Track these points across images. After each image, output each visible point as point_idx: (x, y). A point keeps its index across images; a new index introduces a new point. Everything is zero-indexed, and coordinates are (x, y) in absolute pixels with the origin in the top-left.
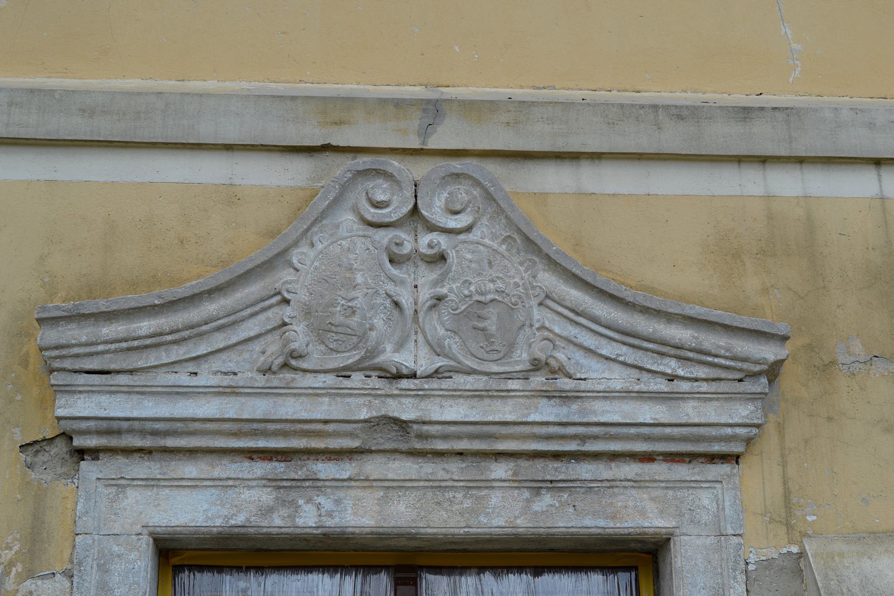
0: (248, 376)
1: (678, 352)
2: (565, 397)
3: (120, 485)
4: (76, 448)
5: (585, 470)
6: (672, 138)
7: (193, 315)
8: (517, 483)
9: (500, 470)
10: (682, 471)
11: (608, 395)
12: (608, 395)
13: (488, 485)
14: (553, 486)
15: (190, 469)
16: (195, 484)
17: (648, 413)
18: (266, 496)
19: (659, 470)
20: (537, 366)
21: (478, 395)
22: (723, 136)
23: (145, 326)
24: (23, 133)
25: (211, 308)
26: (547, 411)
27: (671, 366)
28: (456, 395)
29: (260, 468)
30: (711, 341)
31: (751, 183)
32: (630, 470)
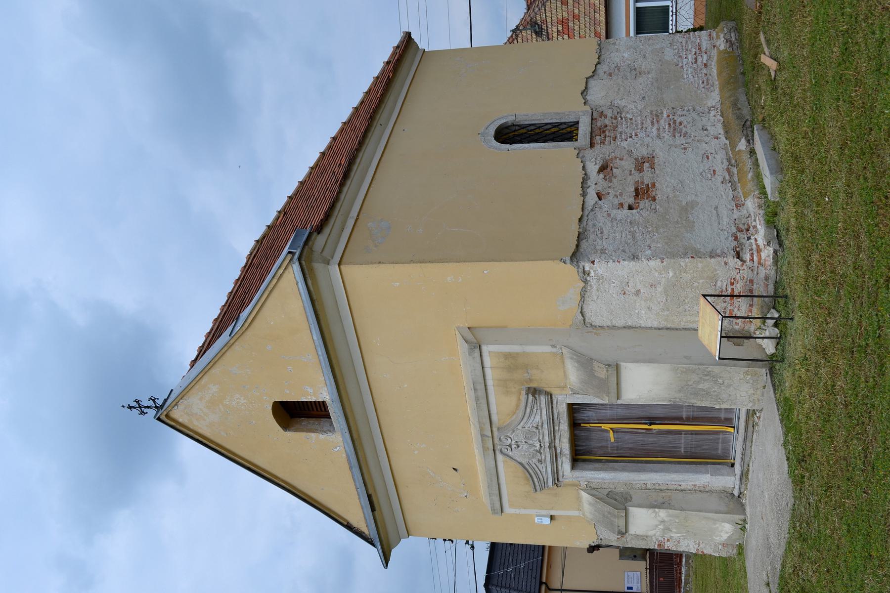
0: (543, 465)
1: (532, 410)
2: (542, 423)
3: (563, 476)
4: (557, 480)
5: (556, 416)
6: (484, 401)
7: (533, 474)
8: (559, 425)
9: (557, 428)
10: (554, 402)
11: (541, 418)
12: (541, 418)
13: (559, 430)
14: (559, 420)
15: (560, 468)
16: (562, 467)
17: (544, 412)
18: (564, 458)
19: (555, 406)
20: (537, 428)
21: (543, 435)
22: (481, 393)
23: (535, 480)
24: (270, 298)
25: (531, 472)
26: (545, 426)
27: (535, 410)
28: (543, 438)
29: (559, 459)
30: (529, 405)
31: (491, 389)
32: (555, 410)
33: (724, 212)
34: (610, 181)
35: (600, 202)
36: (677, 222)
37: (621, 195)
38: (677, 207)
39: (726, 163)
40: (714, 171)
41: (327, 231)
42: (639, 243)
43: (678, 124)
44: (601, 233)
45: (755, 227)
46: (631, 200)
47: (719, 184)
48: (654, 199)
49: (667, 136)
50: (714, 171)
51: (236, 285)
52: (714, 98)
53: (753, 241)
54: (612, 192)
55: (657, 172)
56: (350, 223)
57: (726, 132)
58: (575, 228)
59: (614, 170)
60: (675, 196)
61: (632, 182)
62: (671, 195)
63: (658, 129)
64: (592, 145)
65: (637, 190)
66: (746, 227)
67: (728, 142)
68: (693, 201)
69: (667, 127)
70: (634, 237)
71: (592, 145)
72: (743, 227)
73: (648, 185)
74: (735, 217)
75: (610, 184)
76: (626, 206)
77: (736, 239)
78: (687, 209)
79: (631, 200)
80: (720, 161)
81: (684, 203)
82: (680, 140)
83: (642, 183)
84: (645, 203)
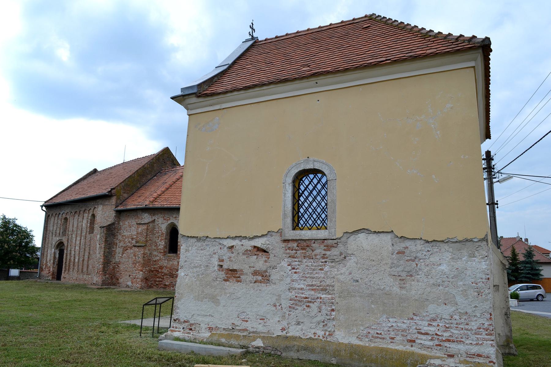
33: (207, 319)
34: (243, 254)
35: (226, 248)
36: (203, 292)
37: (231, 261)
38: (216, 293)
39: (252, 330)
40: (247, 321)
41: (201, 100)
42: (191, 270)
43: (308, 304)
44: (202, 250)
45: (189, 333)
46: (225, 266)
47: (233, 321)
48: (225, 280)
49: (292, 294)
50: (247, 321)
51: (266, 40)
52: (342, 337)
53: (181, 330)
54: (233, 255)
55: (252, 284)
56: (217, 107)
57: (287, 337)
58: (201, 234)
59: (255, 257)
60: (225, 293)
61: (242, 268)
62: (227, 291)
63: (302, 289)
64: (285, 241)
65: (235, 271)
66: (193, 329)
67: (274, 336)
68: (220, 303)
69: (303, 296)
70: (196, 267)
71: (285, 241)
72: (193, 327)
73: (239, 277)
74: (202, 325)
75: (241, 254)
76: (221, 263)
77: (185, 322)
78: (214, 300)
79: (225, 266)
80: (255, 326)
81: (219, 298)
82: (286, 303)
83: (242, 274)
84: (222, 275)
